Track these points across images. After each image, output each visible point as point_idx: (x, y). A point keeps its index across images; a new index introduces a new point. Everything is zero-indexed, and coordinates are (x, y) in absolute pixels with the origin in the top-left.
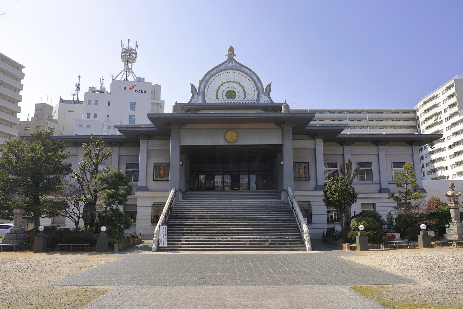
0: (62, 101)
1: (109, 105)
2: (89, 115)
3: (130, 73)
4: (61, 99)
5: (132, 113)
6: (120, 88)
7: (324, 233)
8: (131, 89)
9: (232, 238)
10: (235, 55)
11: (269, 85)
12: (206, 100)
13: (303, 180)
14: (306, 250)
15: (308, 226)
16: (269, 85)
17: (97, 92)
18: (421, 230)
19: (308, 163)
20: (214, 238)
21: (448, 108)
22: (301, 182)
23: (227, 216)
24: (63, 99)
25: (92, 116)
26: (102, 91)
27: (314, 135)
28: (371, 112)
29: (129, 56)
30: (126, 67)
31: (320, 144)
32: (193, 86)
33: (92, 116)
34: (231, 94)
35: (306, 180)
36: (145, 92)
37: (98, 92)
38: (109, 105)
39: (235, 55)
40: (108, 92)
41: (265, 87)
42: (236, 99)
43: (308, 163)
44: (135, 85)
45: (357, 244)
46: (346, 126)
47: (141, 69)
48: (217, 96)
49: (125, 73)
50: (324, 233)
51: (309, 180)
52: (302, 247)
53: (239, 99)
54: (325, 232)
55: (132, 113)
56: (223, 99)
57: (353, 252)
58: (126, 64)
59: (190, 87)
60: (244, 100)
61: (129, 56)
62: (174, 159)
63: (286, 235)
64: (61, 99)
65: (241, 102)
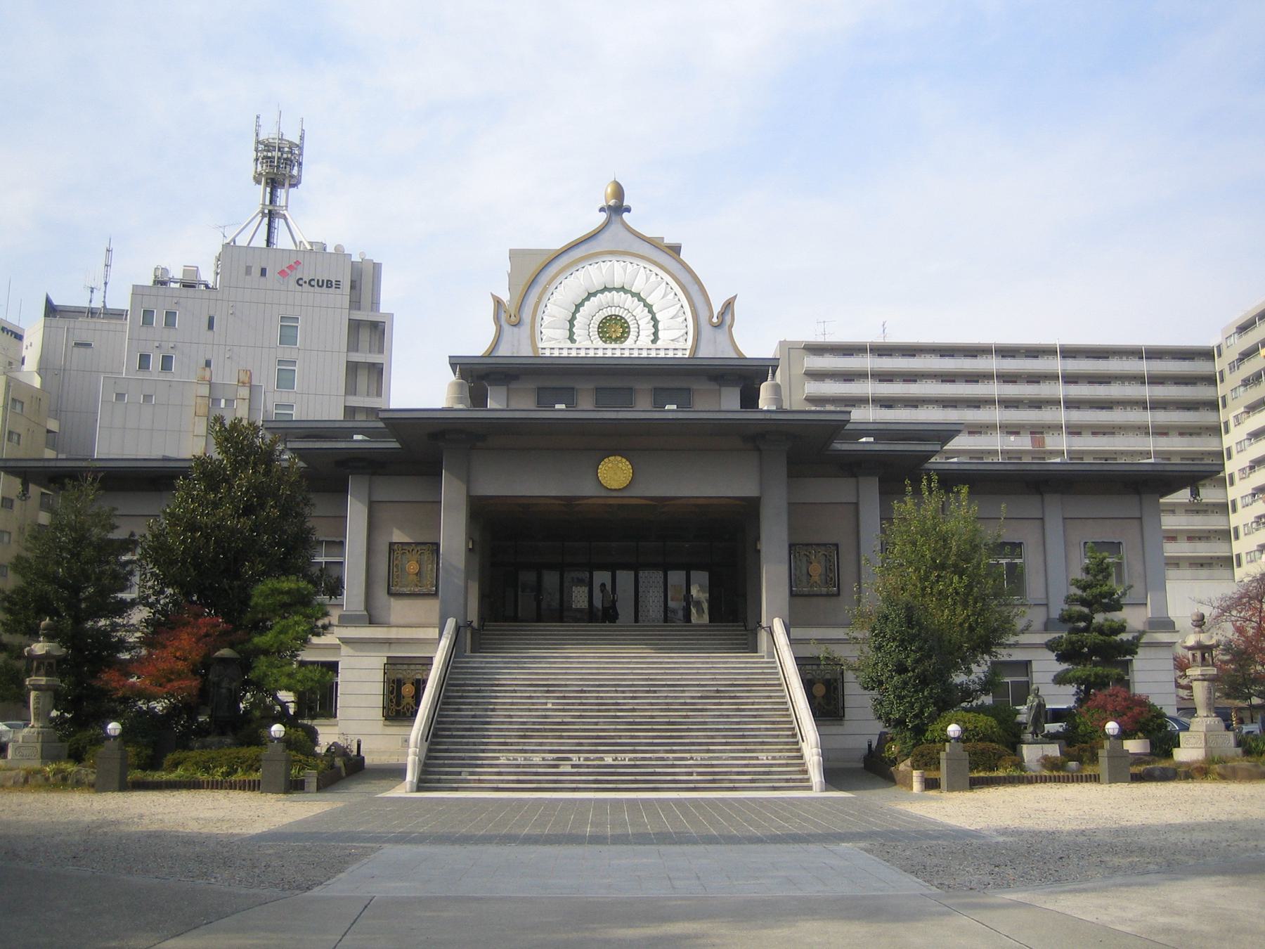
0: (51, 310)
1: (211, 326)
2: (144, 360)
3: (282, 221)
4: (48, 301)
5: (287, 353)
6: (248, 271)
7: (870, 746)
8: (282, 273)
9: (616, 759)
10: (628, 210)
11: (729, 305)
12: (540, 345)
13: (821, 595)
14: (810, 788)
15: (822, 728)
16: (729, 305)
17: (172, 285)
18: (1107, 737)
19: (837, 545)
20: (757, 758)
21: (1242, 389)
22: (815, 599)
23: (602, 698)
24: (56, 301)
25: (155, 362)
26: (189, 279)
27: (856, 466)
28: (1070, 353)
29: (279, 168)
30: (267, 202)
31: (869, 492)
32: (498, 303)
33: (155, 362)
34: (613, 327)
35: (828, 595)
36: (329, 284)
37: (177, 285)
38: (211, 326)
39: (628, 210)
40: (207, 286)
41: (717, 308)
42: (629, 343)
43: (837, 545)
44: (298, 263)
45: (943, 775)
46: (944, 434)
47: (321, 218)
48: (571, 334)
49: (266, 220)
50: (870, 746)
51: (838, 594)
52: (801, 780)
53: (638, 345)
54: (874, 745)
55: (287, 353)
56: (591, 346)
57: (932, 793)
58: (268, 190)
59: (491, 306)
60: (653, 346)
61: (279, 168)
62: (453, 535)
63: (762, 751)
64: (48, 301)
65: (644, 354)
